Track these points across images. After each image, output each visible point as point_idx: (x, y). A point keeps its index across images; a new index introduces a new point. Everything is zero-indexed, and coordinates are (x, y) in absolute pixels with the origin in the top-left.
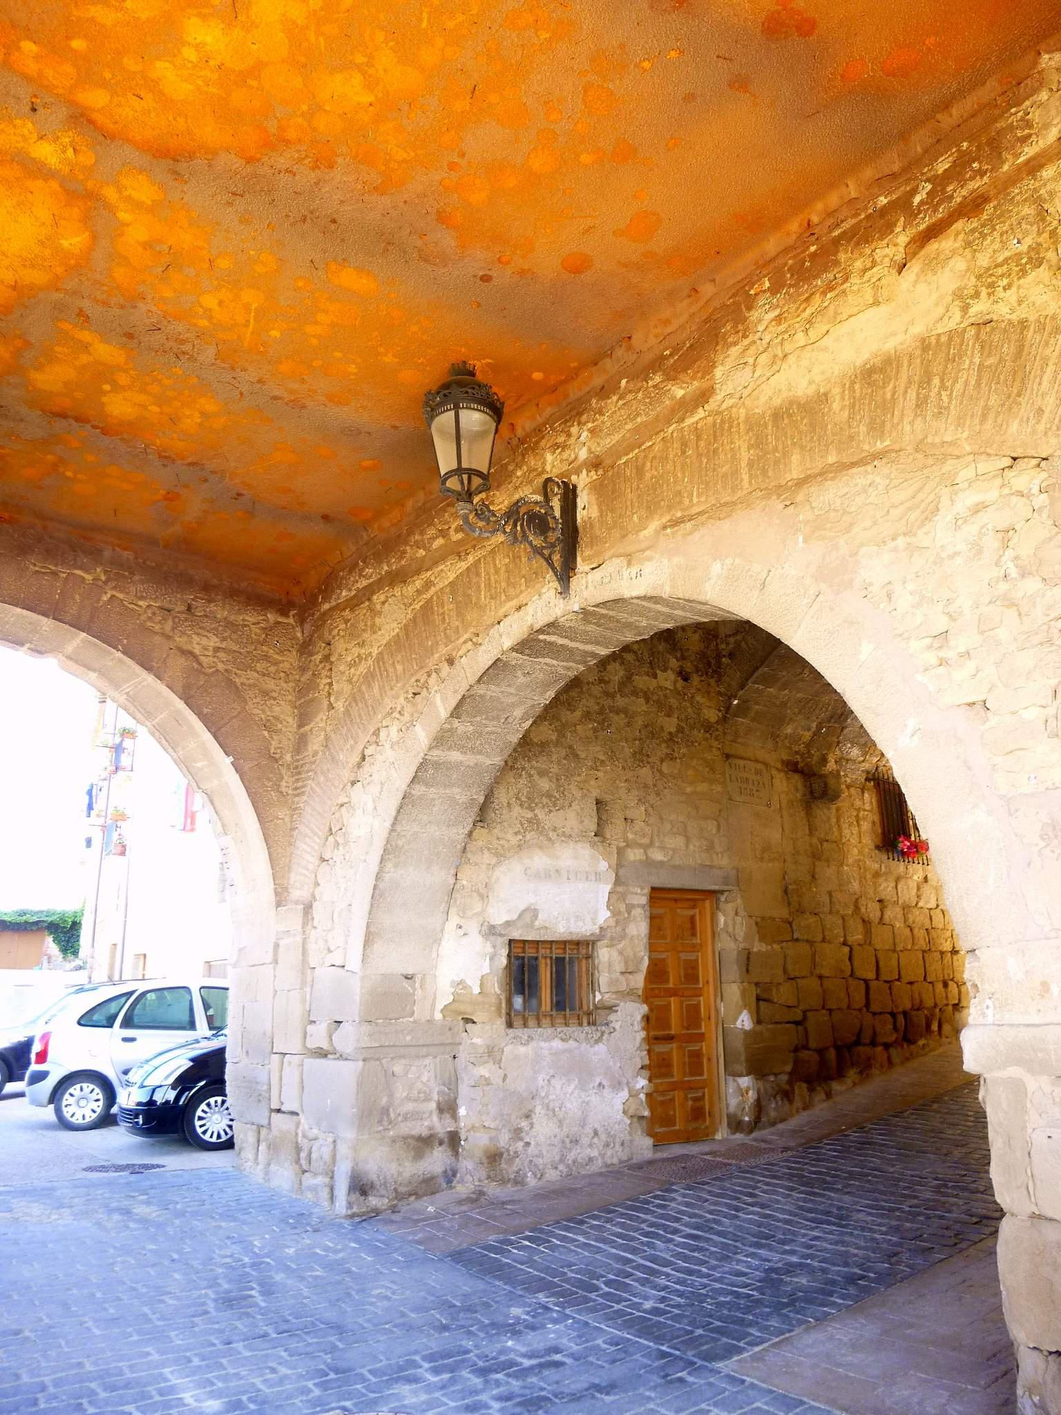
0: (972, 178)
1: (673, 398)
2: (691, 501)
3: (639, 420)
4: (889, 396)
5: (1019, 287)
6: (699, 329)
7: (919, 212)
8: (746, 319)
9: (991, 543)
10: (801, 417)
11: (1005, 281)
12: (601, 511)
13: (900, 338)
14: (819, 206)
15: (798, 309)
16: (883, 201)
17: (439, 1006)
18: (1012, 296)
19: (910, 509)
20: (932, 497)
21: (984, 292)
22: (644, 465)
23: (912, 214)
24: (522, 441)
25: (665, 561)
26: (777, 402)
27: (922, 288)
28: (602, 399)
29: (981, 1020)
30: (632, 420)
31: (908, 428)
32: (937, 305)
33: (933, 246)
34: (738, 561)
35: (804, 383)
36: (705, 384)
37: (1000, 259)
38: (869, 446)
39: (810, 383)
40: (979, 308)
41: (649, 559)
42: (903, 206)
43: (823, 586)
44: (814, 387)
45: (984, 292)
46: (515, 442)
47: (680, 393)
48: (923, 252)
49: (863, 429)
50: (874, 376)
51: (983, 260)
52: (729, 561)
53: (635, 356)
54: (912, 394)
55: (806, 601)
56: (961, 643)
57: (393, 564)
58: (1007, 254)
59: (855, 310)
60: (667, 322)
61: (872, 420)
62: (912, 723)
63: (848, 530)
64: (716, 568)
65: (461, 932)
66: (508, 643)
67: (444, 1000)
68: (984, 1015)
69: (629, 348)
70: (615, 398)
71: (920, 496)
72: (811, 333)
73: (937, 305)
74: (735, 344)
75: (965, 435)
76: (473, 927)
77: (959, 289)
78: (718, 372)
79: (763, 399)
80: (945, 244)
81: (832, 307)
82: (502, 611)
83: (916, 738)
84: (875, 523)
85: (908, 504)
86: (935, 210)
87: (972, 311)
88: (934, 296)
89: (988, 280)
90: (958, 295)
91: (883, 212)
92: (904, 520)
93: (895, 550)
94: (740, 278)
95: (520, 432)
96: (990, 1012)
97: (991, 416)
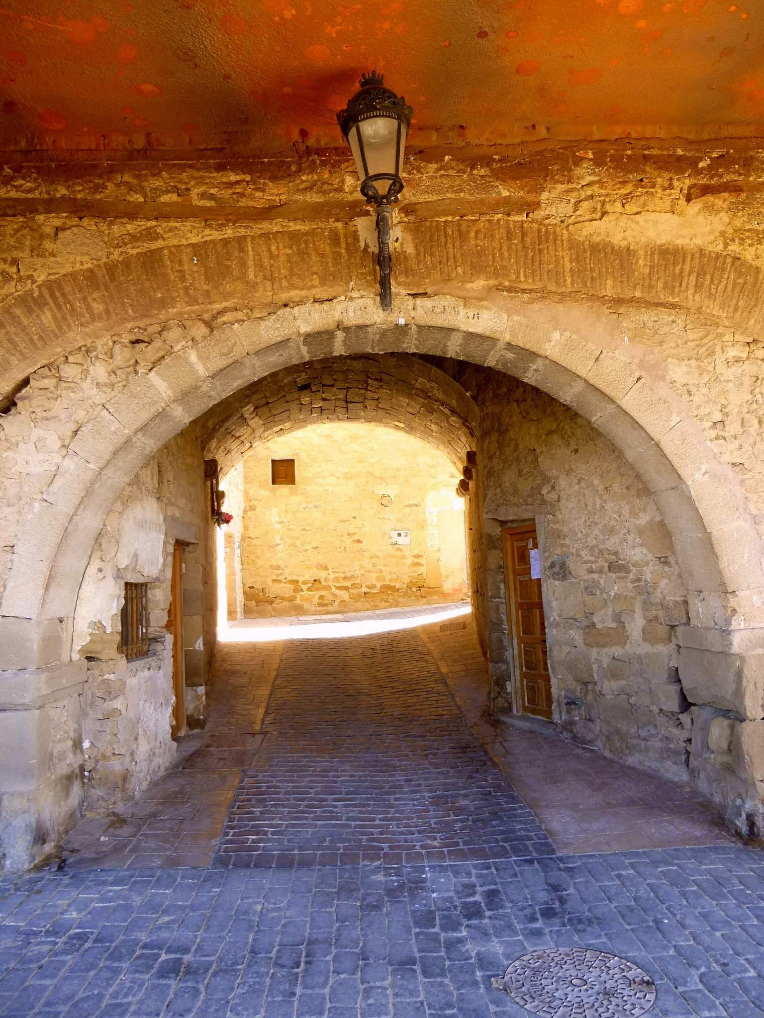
0: (734, 173)
1: (499, 194)
2: (518, 277)
3: (462, 195)
4: (678, 272)
5: (757, 249)
6: (531, 156)
7: (701, 173)
8: (570, 170)
9: (747, 381)
10: (620, 258)
11: (750, 242)
12: (417, 249)
13: (687, 241)
14: (639, 128)
15: (614, 185)
16: (680, 152)
17: (77, 647)
18: (752, 250)
19: (698, 346)
20: (711, 343)
21: (737, 241)
22: (468, 232)
23: (698, 172)
24: (309, 151)
25: (505, 316)
26: (596, 239)
27: (701, 219)
28: (422, 160)
29: (738, 627)
30: (454, 192)
31: (690, 297)
32: (710, 233)
33: (710, 198)
34: (574, 337)
35: (620, 237)
36: (531, 198)
37: (747, 228)
38: (662, 297)
39: (624, 239)
40: (734, 248)
41: (487, 308)
42: (693, 163)
43: (643, 374)
44: (626, 242)
45: (737, 241)
46: (302, 148)
47: (505, 193)
48: (704, 198)
49: (660, 285)
50: (669, 256)
51: (738, 223)
52: (567, 334)
53: (464, 144)
54: (693, 278)
55: (632, 379)
56: (733, 427)
57: (81, 193)
58: (750, 227)
59: (659, 209)
60: (503, 135)
61: (666, 283)
62: (704, 468)
63: (661, 343)
64: (556, 335)
65: (100, 575)
66: (305, 329)
67: (81, 642)
68: (739, 624)
69: (462, 136)
70: (434, 166)
71: (705, 341)
72: (627, 206)
73: (710, 233)
74: (562, 183)
75: (725, 315)
76: (109, 572)
77: (723, 231)
78: (545, 195)
79: (585, 233)
80: (720, 201)
81: (642, 199)
82: (295, 294)
83: (706, 476)
84: (678, 346)
85: (698, 342)
86: (712, 178)
87: (730, 248)
88: (708, 228)
89: (740, 235)
90: (723, 234)
91: (679, 159)
92: (695, 351)
93: (689, 366)
94: (570, 139)
95: (311, 142)
96: (742, 623)
97: (740, 311)
